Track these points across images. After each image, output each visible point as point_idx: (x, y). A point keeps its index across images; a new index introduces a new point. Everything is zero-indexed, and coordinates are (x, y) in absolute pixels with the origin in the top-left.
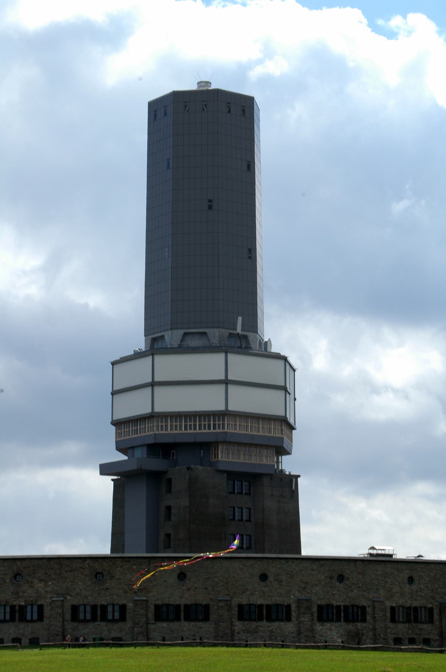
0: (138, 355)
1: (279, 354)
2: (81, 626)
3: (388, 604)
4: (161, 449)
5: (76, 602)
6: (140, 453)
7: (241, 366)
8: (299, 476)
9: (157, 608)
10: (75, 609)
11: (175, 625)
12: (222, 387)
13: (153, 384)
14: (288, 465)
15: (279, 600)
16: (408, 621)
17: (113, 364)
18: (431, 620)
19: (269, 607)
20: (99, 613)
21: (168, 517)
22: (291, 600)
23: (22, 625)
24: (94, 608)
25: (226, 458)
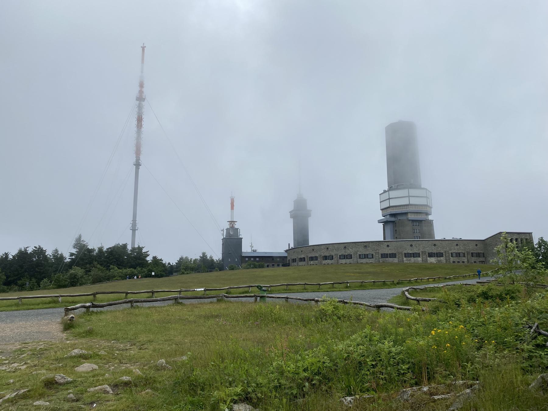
1: (40, 252)
3: (450, 252)
4: (392, 215)
5: (360, 253)
6: (388, 217)
7: (413, 192)
8: (80, 236)
11: (387, 259)
12: (408, 198)
13: (389, 199)
14: (430, 218)
15: (417, 252)
18: (464, 256)
19: (413, 254)
22: (420, 252)
25: (411, 217)
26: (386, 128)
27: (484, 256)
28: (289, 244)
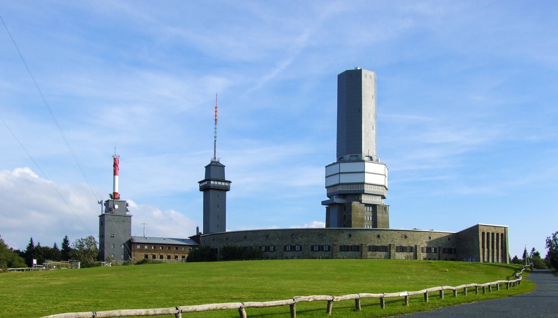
0: (334, 164)
2: (315, 253)
3: (421, 246)
4: (343, 195)
9: (341, 246)
10: (312, 247)
16: (448, 253)
17: (326, 167)
20: (321, 248)
21: (345, 219)
23: (294, 252)
24: (319, 246)
26: (338, 76)
27: (455, 253)
28: (198, 228)
